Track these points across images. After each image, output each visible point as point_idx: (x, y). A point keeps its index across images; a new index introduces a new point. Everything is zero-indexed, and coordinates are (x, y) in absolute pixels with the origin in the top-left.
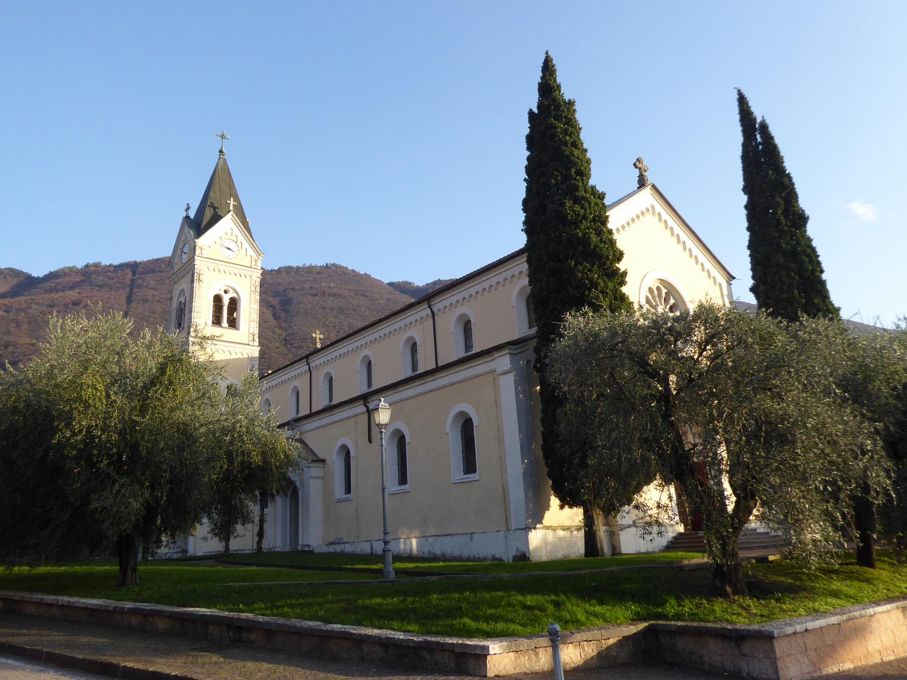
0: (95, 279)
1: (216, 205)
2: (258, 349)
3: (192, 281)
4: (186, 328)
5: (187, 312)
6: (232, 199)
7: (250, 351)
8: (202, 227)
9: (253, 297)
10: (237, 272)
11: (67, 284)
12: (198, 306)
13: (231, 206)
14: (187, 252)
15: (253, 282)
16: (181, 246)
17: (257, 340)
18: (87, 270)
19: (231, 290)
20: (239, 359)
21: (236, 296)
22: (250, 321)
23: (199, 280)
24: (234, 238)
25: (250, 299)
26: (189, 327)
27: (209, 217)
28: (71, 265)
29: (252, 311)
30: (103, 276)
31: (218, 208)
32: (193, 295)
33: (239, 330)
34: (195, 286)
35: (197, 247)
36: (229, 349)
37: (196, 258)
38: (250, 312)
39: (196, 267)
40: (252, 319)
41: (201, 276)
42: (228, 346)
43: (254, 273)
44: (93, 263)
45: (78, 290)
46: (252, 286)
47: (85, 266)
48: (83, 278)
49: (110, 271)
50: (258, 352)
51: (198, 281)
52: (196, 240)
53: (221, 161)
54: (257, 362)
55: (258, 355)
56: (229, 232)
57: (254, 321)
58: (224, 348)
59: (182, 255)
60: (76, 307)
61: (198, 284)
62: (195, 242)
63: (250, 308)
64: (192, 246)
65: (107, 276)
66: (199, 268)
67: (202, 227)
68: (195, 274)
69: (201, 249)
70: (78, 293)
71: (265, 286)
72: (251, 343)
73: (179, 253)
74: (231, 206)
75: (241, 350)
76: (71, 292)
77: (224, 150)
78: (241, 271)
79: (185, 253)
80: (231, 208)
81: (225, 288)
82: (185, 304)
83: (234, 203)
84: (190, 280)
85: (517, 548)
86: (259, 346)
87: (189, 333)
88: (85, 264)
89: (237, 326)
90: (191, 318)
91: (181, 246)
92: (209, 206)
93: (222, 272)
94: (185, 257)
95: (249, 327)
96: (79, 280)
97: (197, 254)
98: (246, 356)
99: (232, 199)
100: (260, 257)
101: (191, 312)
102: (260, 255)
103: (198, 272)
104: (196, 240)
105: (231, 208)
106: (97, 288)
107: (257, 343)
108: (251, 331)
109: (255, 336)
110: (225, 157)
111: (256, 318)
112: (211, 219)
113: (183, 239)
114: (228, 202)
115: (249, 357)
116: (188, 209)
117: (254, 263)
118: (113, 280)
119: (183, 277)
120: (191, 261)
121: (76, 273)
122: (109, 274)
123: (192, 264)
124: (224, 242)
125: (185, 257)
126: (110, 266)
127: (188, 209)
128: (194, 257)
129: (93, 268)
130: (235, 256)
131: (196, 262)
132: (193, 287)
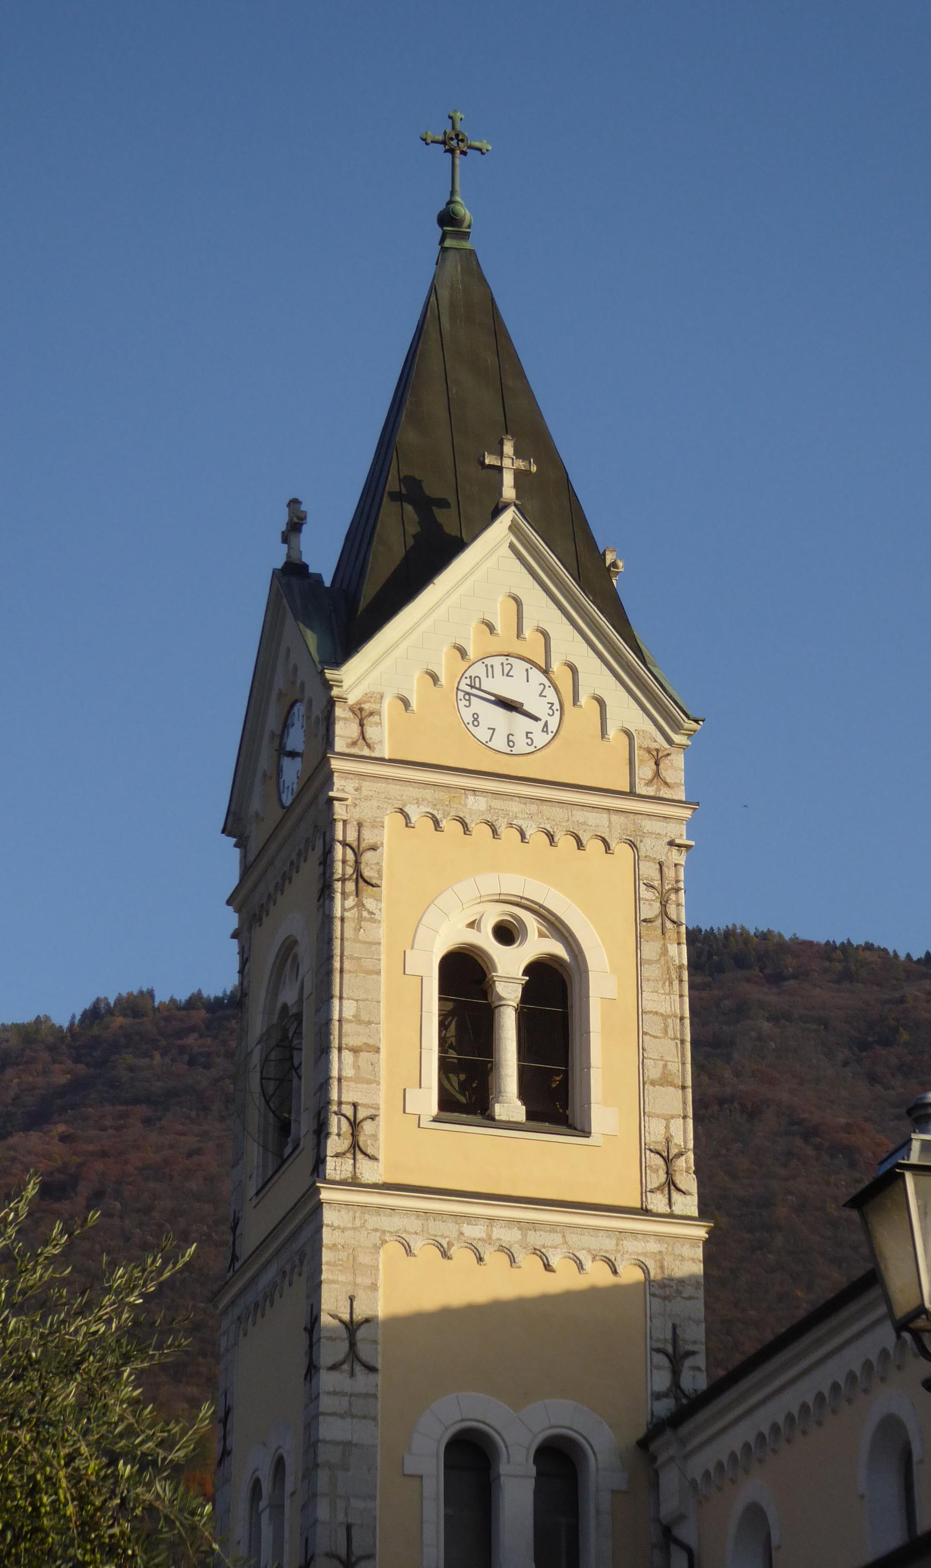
0: (131, 1069)
1: (434, 489)
2: (700, 1232)
3: (325, 892)
4: (308, 1142)
5: (305, 1057)
6: (508, 448)
7: (653, 1246)
8: (363, 604)
9: (650, 950)
10: (557, 818)
11: (16, 1098)
12: (357, 1019)
13: (508, 479)
14: (300, 748)
15: (649, 871)
16: (272, 723)
17: (688, 1182)
18: (95, 1031)
19: (532, 923)
20: (594, 1294)
21: (558, 949)
22: (643, 1083)
23: (359, 877)
24: (533, 647)
25: (640, 963)
26: (321, 1132)
27: (399, 553)
28: (25, 1017)
29: (653, 1025)
30: (162, 1055)
31: (443, 503)
32: (330, 957)
33: (586, 1133)
34: (338, 912)
35: (339, 711)
36: (535, 1239)
37: (335, 764)
38: (641, 1033)
39: (339, 810)
40: (654, 1072)
41: (368, 857)
42: (534, 1226)
43: (649, 825)
44: (119, 999)
45: (61, 1128)
46: (645, 893)
47: (85, 1014)
48: (81, 1068)
49: (192, 1029)
50: (699, 1253)
51: (350, 886)
52: (329, 674)
53: (453, 264)
54: (697, 1308)
55: (698, 1269)
56: (502, 618)
57: (665, 1080)
58: (510, 1236)
59: (279, 770)
60: (57, 1206)
61: (351, 902)
62: (327, 686)
63: (641, 1012)
64: (317, 711)
65: (182, 1050)
66: (355, 815)
67: (363, 604)
68: (339, 850)
69: (361, 715)
70: (63, 1138)
71: (905, 1036)
72: (658, 1203)
73: (265, 762)
74: (508, 479)
75: (607, 1244)
76: (34, 1139)
77: (463, 210)
78: (580, 815)
79: (293, 754)
80: (509, 492)
81: (493, 916)
82: (299, 1017)
83: (521, 464)
84: (316, 888)
85: (795, 934)
86: (704, 1212)
87: (320, 1161)
88: (87, 1004)
89: (577, 1118)
90: (324, 1085)
91: (272, 723)
92: (396, 497)
93: (481, 832)
94: (292, 771)
95: (643, 1113)
96: (64, 1079)
97: (340, 745)
98: (630, 1275)
99: (508, 448)
100: (677, 738)
101: (325, 1050)
102: (677, 727)
103: (351, 837)
104: (329, 674)
105: (509, 492)
106: (143, 1110)
107: (688, 1204)
108: (656, 1132)
109: (681, 1163)
110: (467, 245)
111: (675, 1067)
112: (406, 559)
113: (279, 683)
114: (489, 460)
115: (648, 1281)
116: (295, 526)
117: (645, 771)
118: (207, 1066)
119: (286, 878)
120: (316, 783)
121: (52, 1048)
122: (191, 1040)
123: (322, 800)
124: (478, 670)
125: (292, 771)
126: (195, 1001)
127: (295, 526)
128: (325, 761)
129: (120, 1020)
130: (541, 739)
131: (341, 787)
132: (327, 920)
